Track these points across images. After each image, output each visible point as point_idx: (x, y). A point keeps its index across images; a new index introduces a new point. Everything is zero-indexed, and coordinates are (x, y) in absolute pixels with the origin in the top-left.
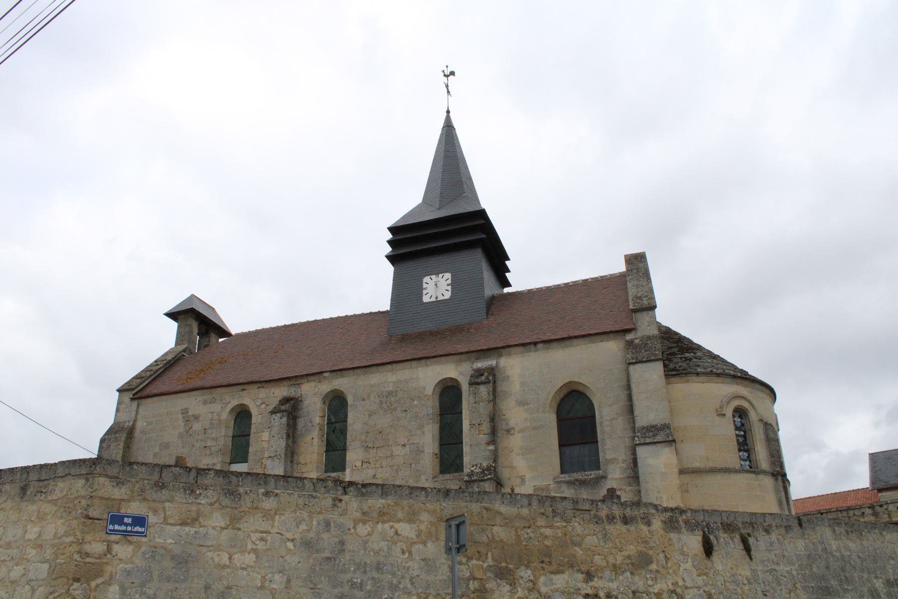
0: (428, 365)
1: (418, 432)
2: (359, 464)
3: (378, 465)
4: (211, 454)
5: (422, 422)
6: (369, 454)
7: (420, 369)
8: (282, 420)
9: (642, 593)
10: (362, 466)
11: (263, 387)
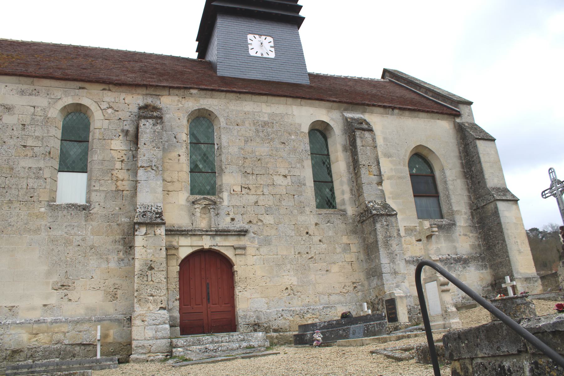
0: (302, 105)
1: (298, 165)
2: (238, 189)
4: (35, 156)
5: (301, 156)
7: (294, 107)
8: (156, 127)
9: (149, 340)
11: (110, 90)
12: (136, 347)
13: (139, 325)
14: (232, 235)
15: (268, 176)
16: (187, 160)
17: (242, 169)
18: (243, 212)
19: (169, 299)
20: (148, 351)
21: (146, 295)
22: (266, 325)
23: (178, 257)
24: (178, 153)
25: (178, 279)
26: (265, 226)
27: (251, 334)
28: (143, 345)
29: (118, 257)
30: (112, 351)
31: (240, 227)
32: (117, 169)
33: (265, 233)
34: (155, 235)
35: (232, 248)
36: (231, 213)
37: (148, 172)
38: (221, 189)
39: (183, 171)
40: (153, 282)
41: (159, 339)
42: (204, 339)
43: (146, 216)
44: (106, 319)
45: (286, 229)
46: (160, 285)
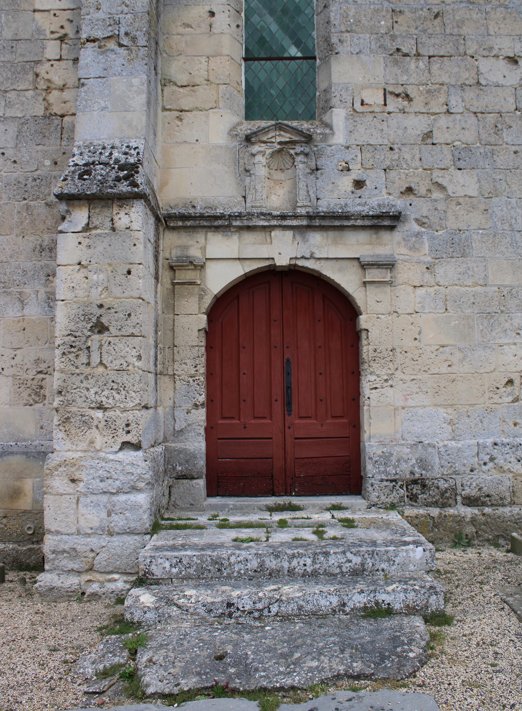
3: (436, 106)
6: (406, 71)
9: (88, 535)
10: (385, 105)
12: (54, 552)
13: (61, 491)
14: (354, 228)
15: (462, 60)
16: (234, 26)
17: (387, 42)
18: (388, 163)
19: (177, 405)
20: (87, 567)
21: (84, 405)
22: (443, 485)
23: (204, 291)
24: (207, 8)
25: (203, 349)
26: (454, 203)
27: (387, 552)
28: (74, 549)
29: (48, 290)
30: (30, 532)
31: (379, 206)
32: (50, 60)
33: (452, 224)
34: (113, 229)
35: (356, 263)
36: (355, 167)
37: (109, 54)
38: (327, 101)
39: (221, 55)
40: (106, 367)
41: (118, 534)
42: (233, 559)
43: (90, 175)
44: (15, 449)
45: (512, 212)
46: (124, 378)
